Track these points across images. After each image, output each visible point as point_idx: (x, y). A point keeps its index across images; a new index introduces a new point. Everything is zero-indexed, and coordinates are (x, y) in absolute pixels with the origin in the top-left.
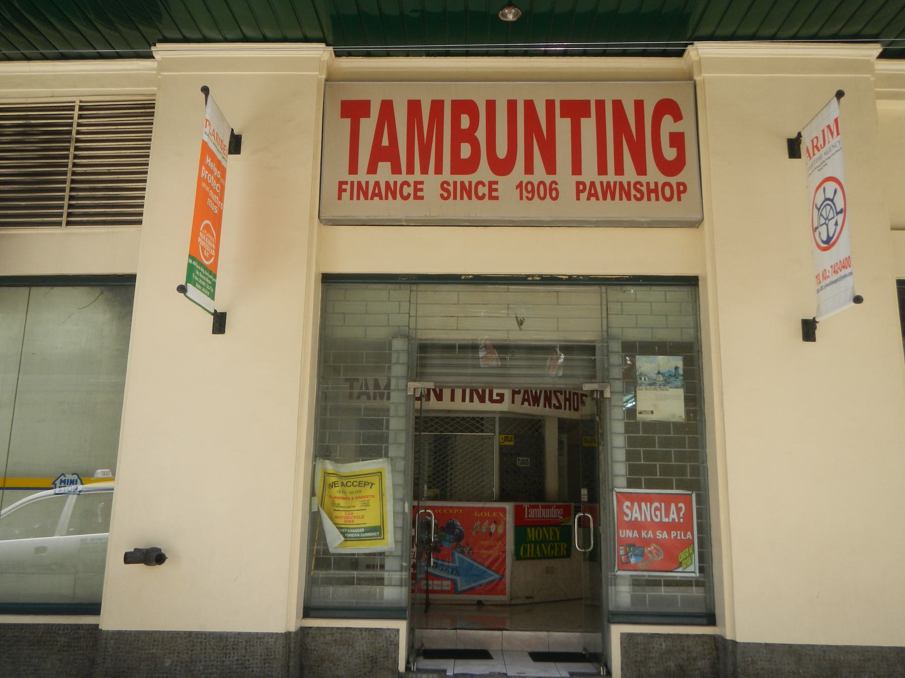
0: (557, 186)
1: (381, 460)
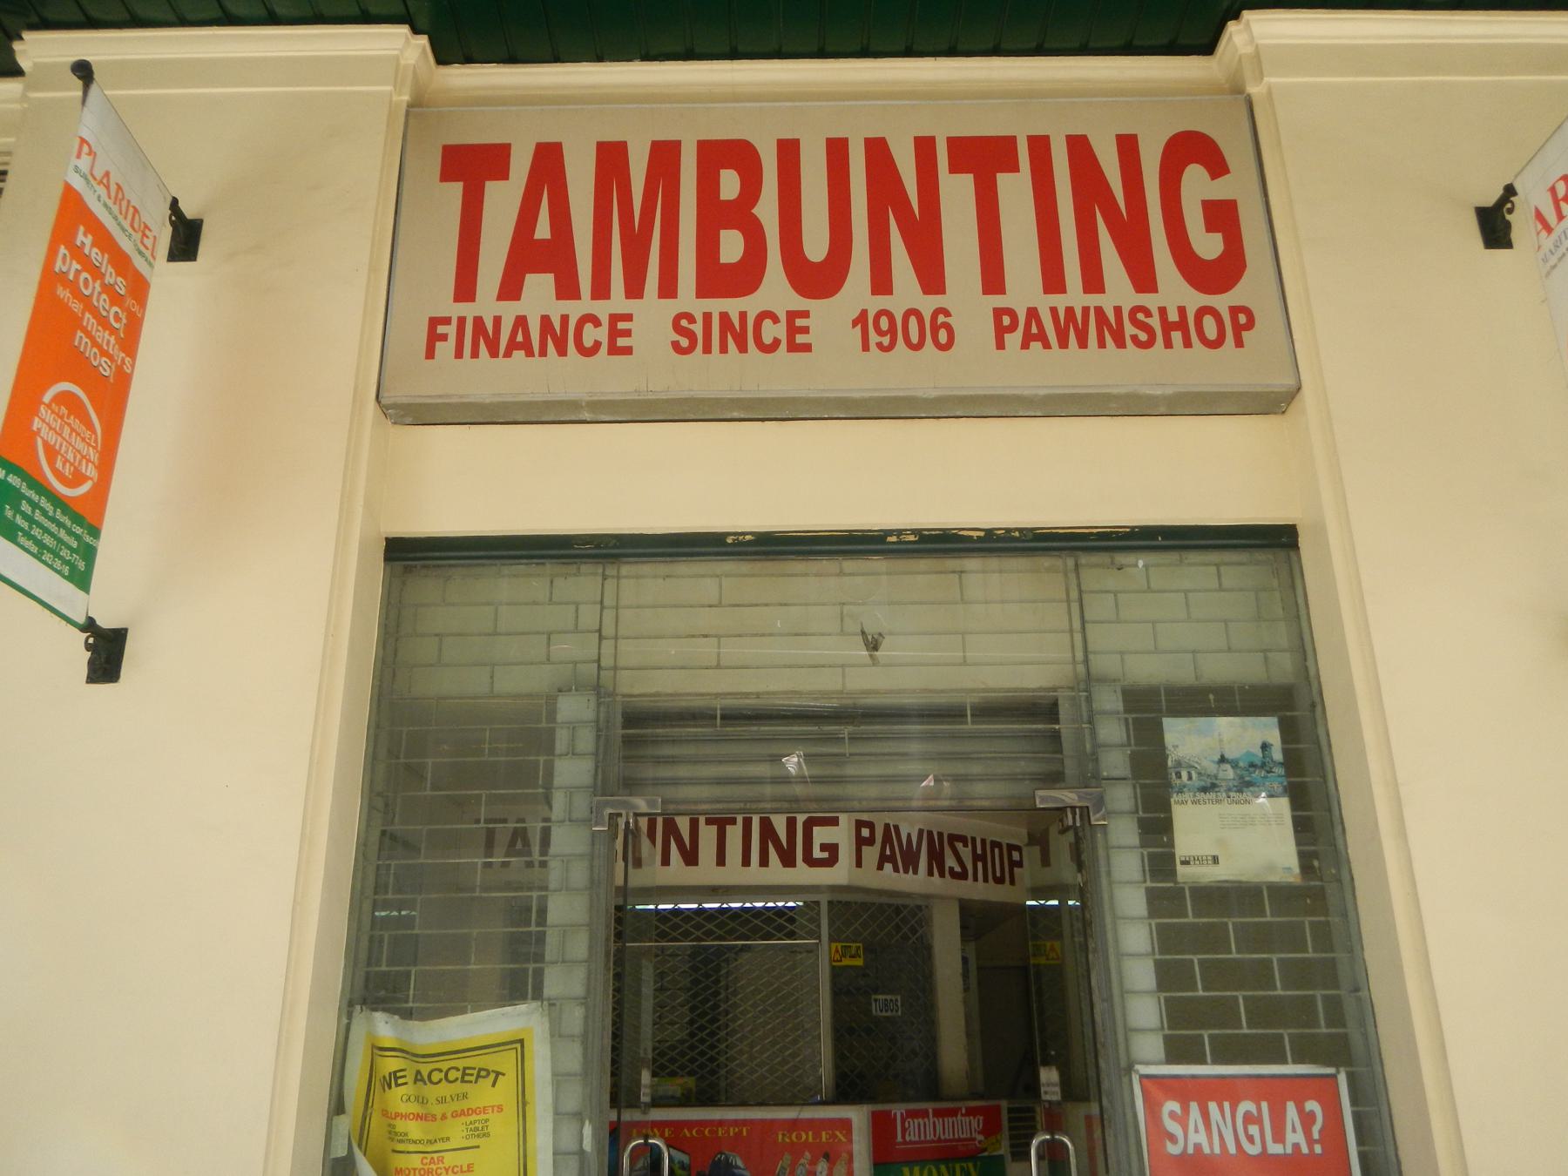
0: (948, 320)
1: (522, 1007)
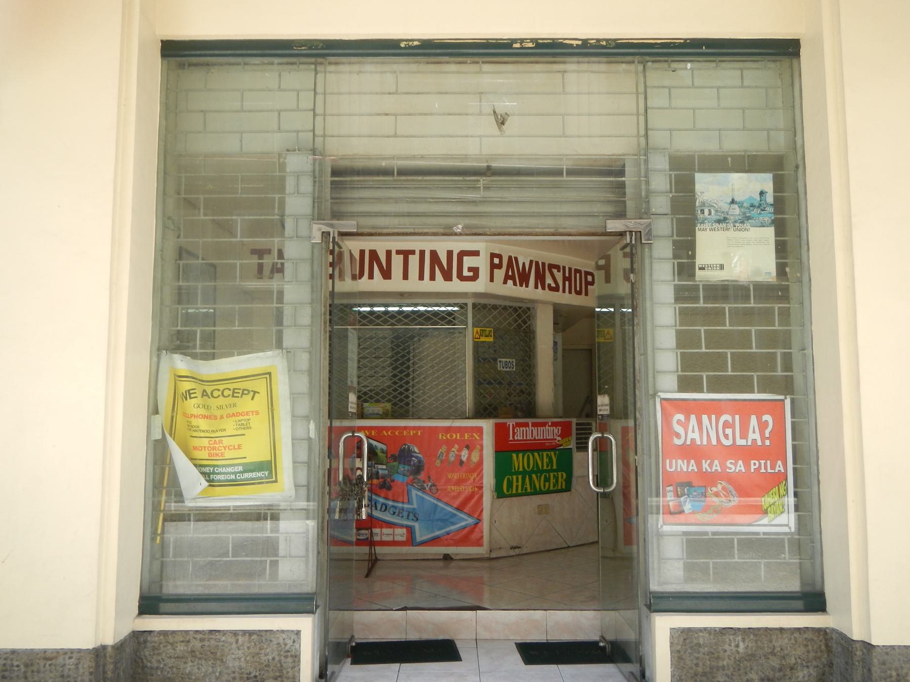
1: (270, 353)
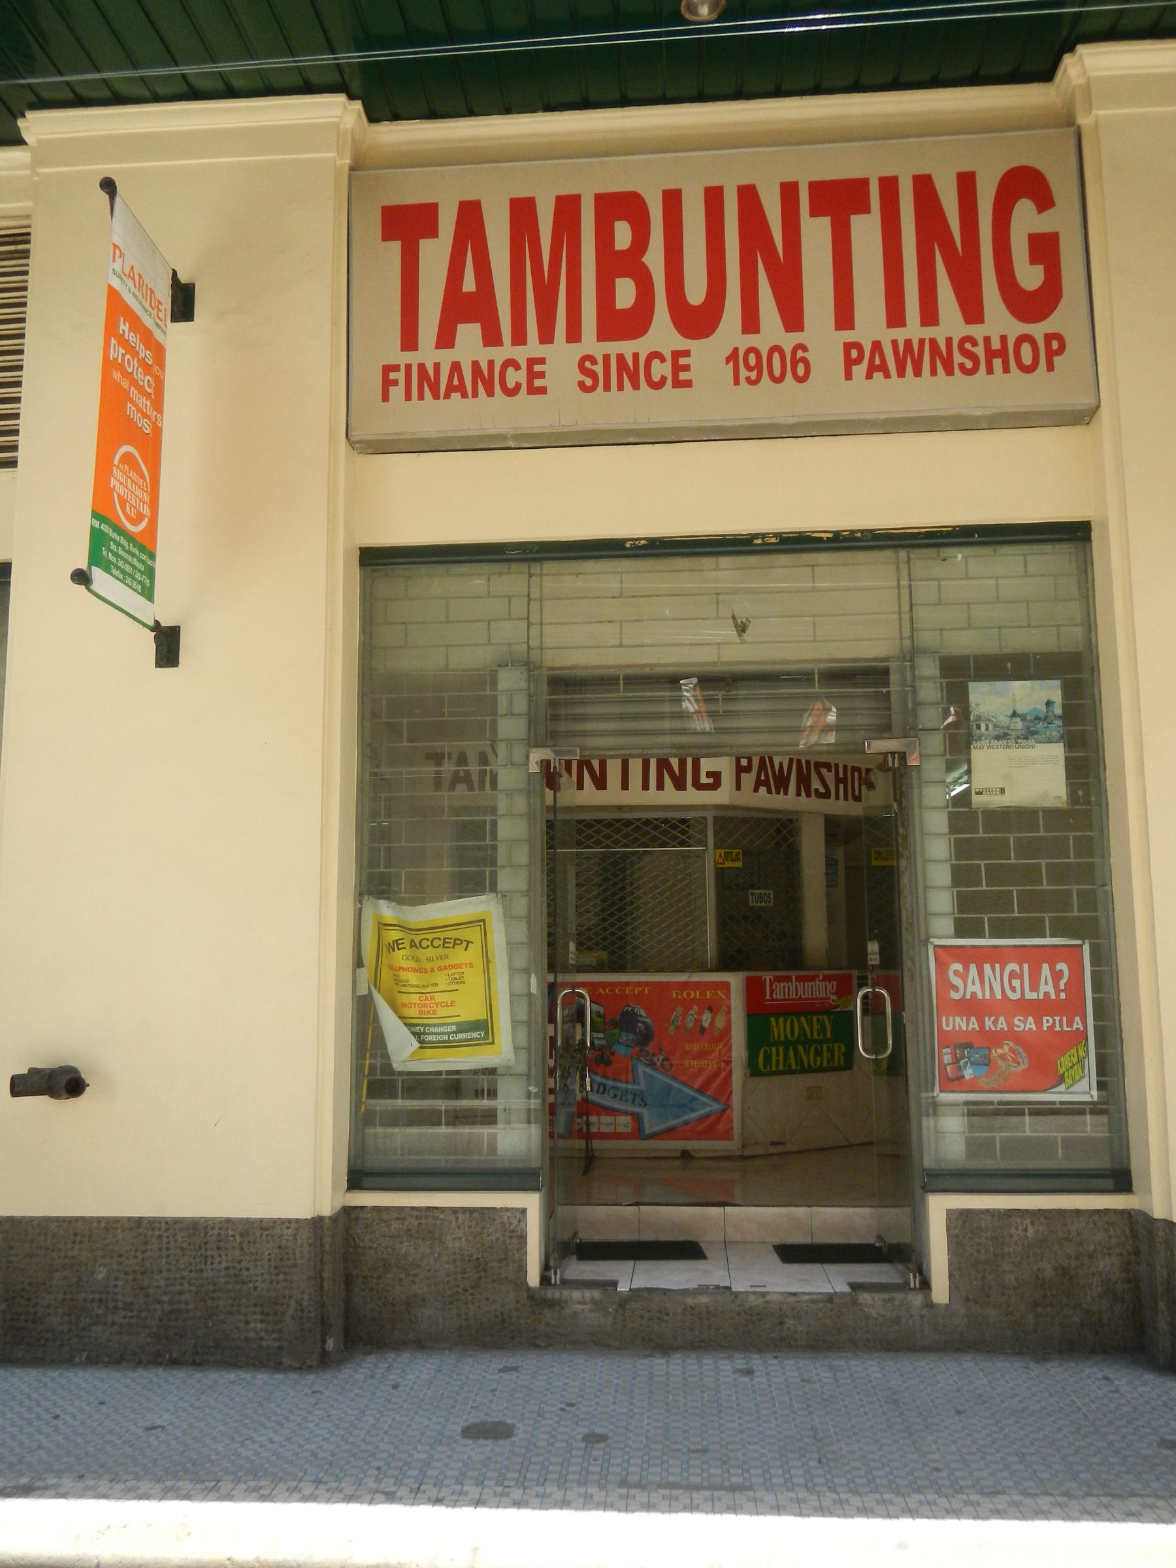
1: (483, 898)
